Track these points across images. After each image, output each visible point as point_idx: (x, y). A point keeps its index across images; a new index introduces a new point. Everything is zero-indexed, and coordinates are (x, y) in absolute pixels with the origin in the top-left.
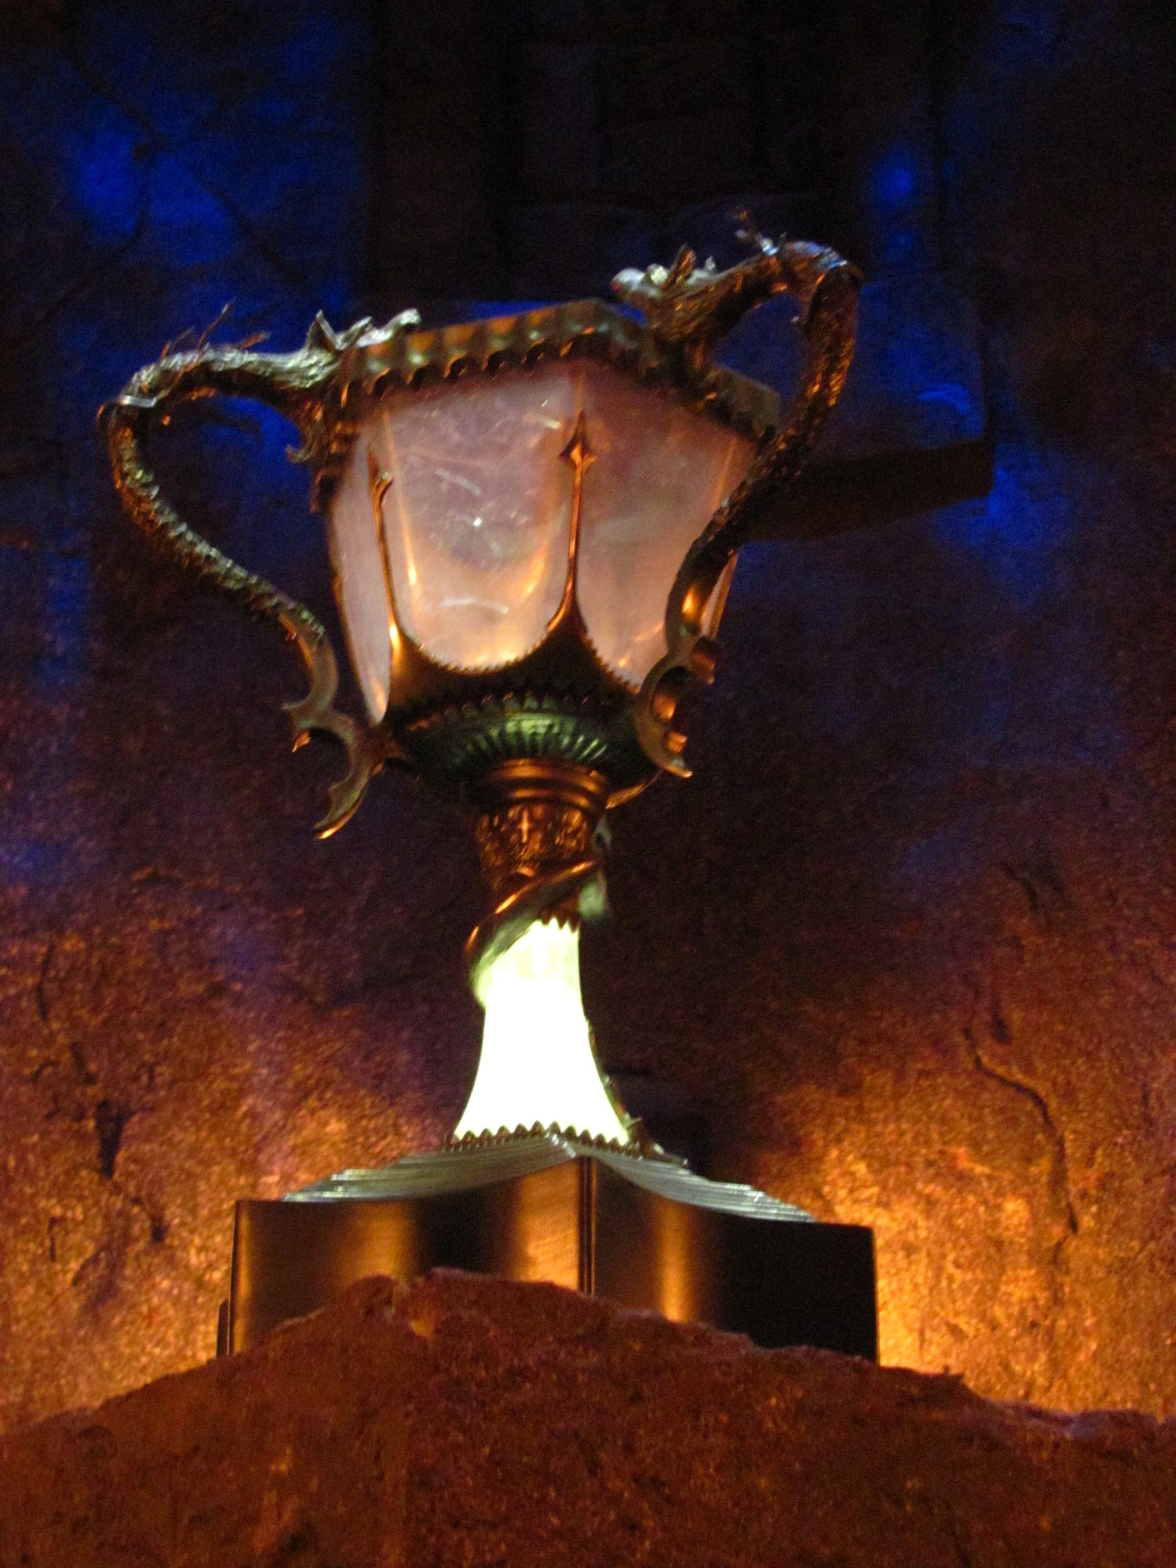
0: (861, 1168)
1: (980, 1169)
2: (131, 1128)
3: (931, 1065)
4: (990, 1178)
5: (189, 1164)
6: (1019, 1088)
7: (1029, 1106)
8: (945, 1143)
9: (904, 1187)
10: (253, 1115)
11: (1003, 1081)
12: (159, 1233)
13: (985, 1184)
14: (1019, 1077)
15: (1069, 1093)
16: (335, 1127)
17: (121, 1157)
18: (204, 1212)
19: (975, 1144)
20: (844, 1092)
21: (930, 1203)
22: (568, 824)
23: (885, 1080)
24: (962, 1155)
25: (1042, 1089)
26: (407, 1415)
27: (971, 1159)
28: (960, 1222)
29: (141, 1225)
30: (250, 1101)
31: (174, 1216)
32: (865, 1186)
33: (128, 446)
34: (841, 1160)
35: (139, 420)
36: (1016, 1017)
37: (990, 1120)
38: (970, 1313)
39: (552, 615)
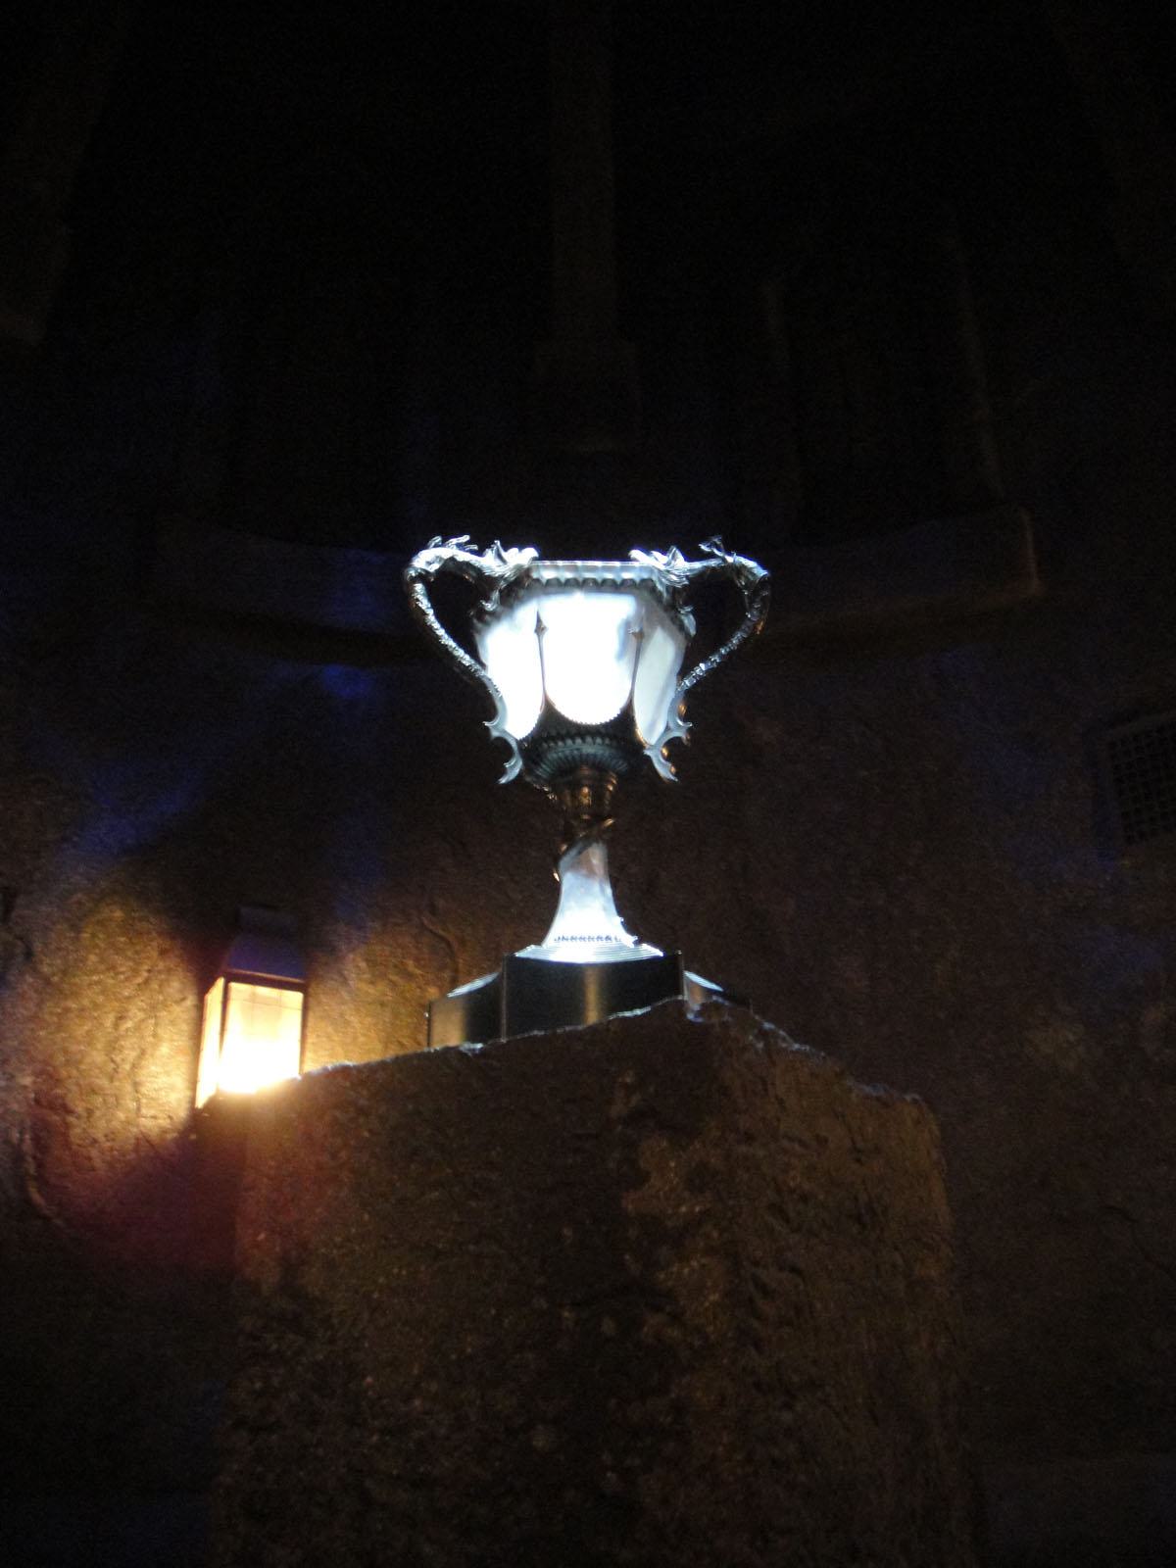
0: (363, 965)
1: (418, 972)
2: (21, 900)
3: (400, 921)
4: (422, 975)
5: (47, 923)
6: (442, 938)
7: (443, 945)
8: (404, 958)
9: (383, 976)
10: (79, 903)
11: (431, 931)
12: (29, 954)
13: (421, 978)
14: (441, 932)
15: (462, 942)
16: (118, 914)
17: (14, 915)
18: (52, 947)
19: (417, 960)
20: (360, 928)
21: (394, 985)
22: (578, 808)
23: (377, 925)
24: (410, 964)
25: (451, 939)
26: (794, 1178)
27: (416, 967)
28: (408, 995)
29: (20, 949)
30: (79, 895)
31: (38, 946)
32: (364, 973)
33: (419, 587)
34: (354, 960)
35: (423, 577)
36: (441, 903)
37: (425, 950)
38: (409, 1037)
39: (622, 703)
